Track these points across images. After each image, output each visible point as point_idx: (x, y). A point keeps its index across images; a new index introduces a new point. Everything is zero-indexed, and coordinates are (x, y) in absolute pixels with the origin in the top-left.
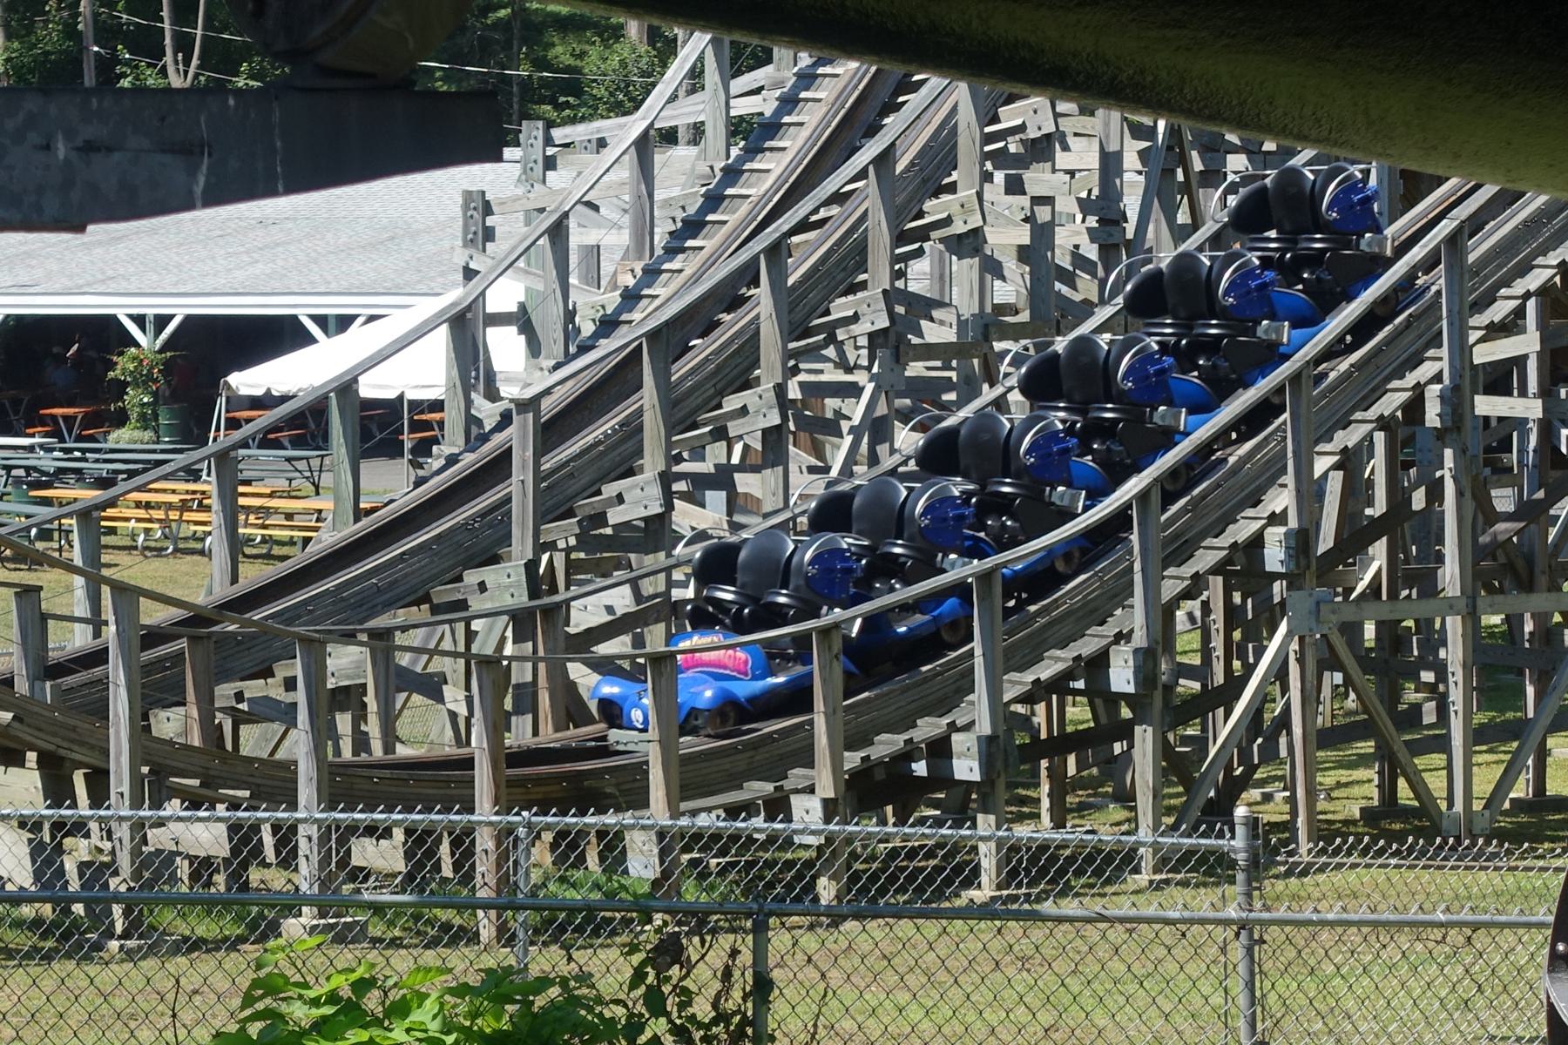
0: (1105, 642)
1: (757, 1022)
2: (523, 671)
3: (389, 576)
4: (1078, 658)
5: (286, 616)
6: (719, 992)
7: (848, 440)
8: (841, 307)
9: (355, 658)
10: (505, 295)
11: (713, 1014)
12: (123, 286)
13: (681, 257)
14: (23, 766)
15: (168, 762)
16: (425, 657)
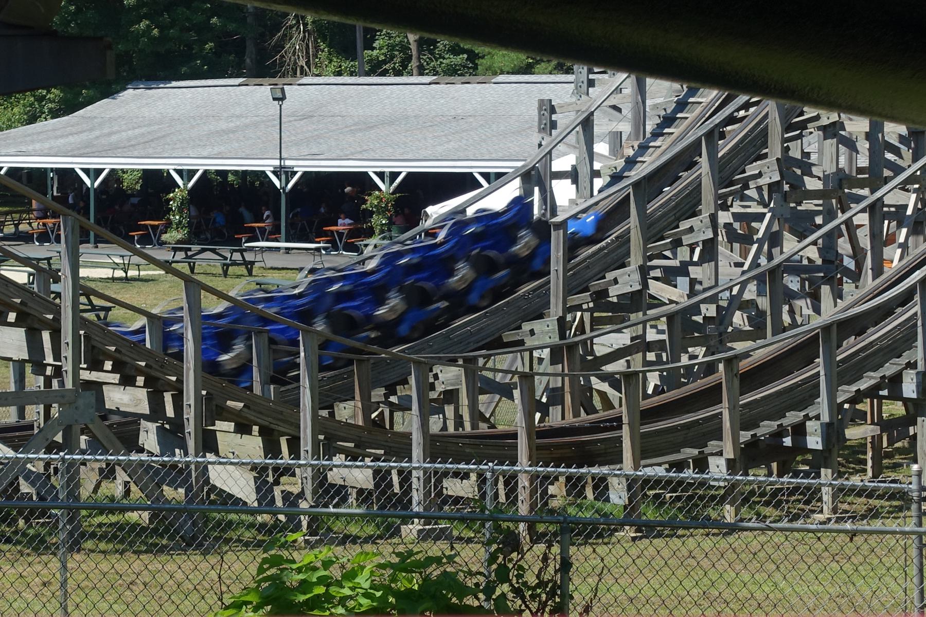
0: (900, 368)
1: (564, 586)
2: (556, 382)
3: (477, 326)
4: (883, 377)
5: (416, 348)
6: (541, 568)
7: (755, 246)
8: (752, 169)
9: (455, 373)
10: (562, 164)
11: (537, 581)
12: (372, 155)
13: (661, 138)
14: (251, 434)
15: (336, 433)
16: (510, 376)
